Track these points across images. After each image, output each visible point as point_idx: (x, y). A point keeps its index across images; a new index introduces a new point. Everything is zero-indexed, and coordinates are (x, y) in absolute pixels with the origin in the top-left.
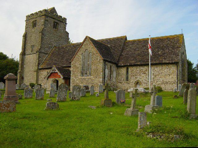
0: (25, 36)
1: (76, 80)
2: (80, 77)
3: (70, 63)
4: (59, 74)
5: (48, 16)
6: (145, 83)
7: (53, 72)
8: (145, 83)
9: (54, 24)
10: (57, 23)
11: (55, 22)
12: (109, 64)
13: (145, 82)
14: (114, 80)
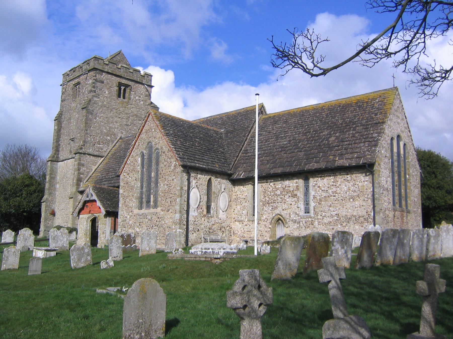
0: (59, 119)
1: (129, 217)
2: (136, 211)
3: (119, 176)
4: (99, 203)
5: (103, 71)
6: (295, 221)
7: (88, 199)
8: (295, 221)
9: (120, 89)
10: (127, 86)
11: (120, 85)
12: (203, 178)
13: (296, 218)
14: (222, 215)
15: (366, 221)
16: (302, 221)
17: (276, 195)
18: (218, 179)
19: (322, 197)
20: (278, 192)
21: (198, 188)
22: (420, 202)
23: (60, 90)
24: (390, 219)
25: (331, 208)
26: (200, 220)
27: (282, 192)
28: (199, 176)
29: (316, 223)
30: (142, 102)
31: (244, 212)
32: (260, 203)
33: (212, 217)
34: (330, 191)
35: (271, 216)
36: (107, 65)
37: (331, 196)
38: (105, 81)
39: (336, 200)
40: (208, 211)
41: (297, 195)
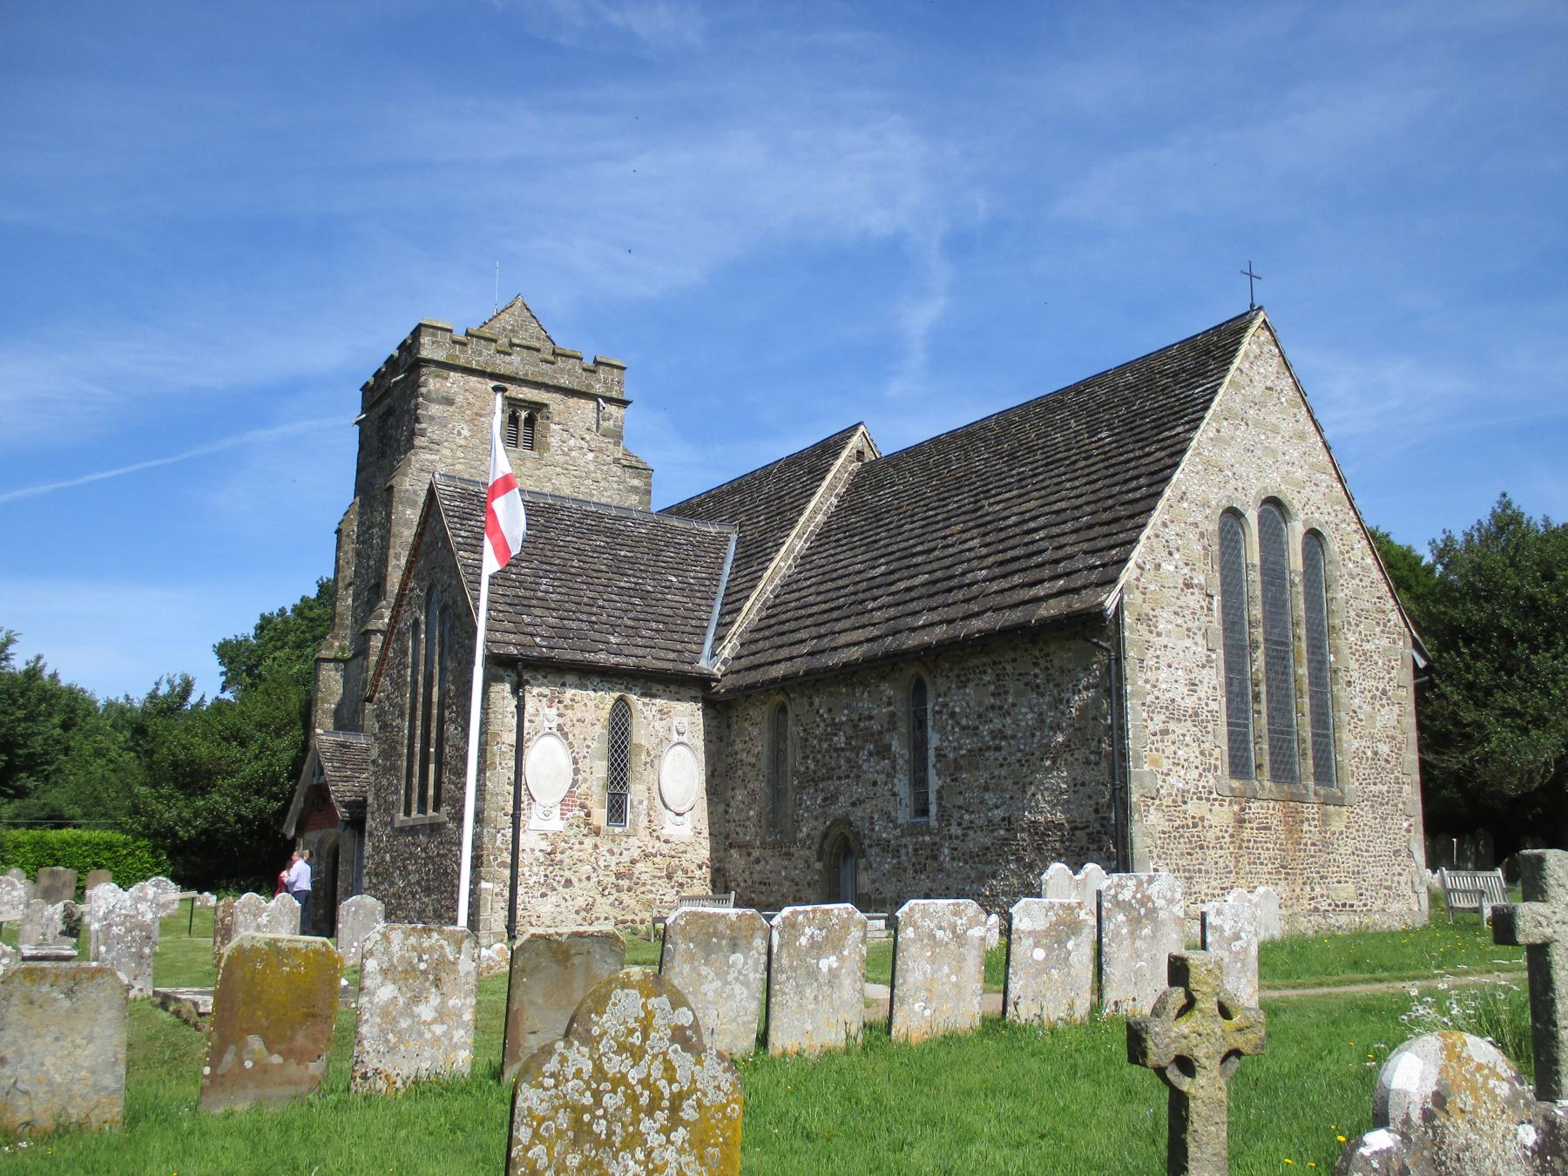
10: (537, 408)
11: (513, 404)
12: (594, 705)
15: (1095, 846)
16: (905, 846)
17: (836, 750)
18: (657, 701)
19: (963, 752)
20: (840, 740)
21: (565, 735)
22: (1412, 757)
23: (354, 434)
24: (1211, 835)
25: (987, 796)
26: (577, 846)
27: (852, 737)
28: (570, 693)
29: (946, 851)
30: (591, 456)
31: (752, 813)
32: (792, 781)
33: (628, 836)
34: (985, 730)
35: (822, 828)
36: (464, 344)
37: (989, 748)
38: (459, 399)
39: (1002, 765)
40: (617, 810)
41: (890, 749)
